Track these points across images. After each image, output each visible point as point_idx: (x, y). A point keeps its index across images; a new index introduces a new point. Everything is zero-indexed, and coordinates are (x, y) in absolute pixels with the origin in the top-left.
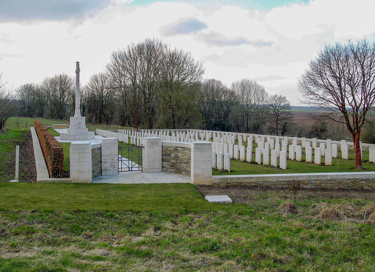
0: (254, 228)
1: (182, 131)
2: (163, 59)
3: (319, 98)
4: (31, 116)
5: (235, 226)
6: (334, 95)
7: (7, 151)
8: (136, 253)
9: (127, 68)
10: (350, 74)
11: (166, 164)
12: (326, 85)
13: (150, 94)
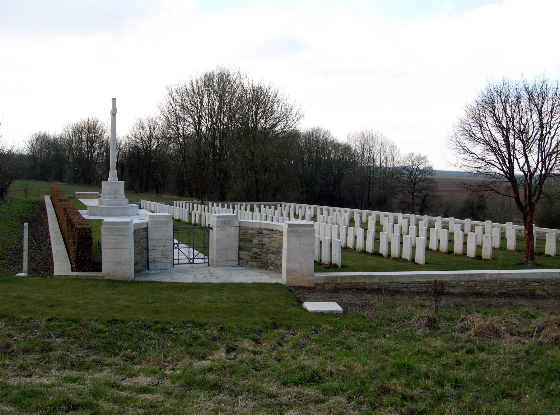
0: (374, 350)
1: (269, 205)
2: (243, 94)
3: (476, 159)
4: (45, 180)
5: (346, 348)
6: (498, 154)
7: (11, 230)
8: (199, 384)
9: (187, 107)
10: (523, 124)
11: (244, 254)
12: (487, 139)
13: (222, 147)
